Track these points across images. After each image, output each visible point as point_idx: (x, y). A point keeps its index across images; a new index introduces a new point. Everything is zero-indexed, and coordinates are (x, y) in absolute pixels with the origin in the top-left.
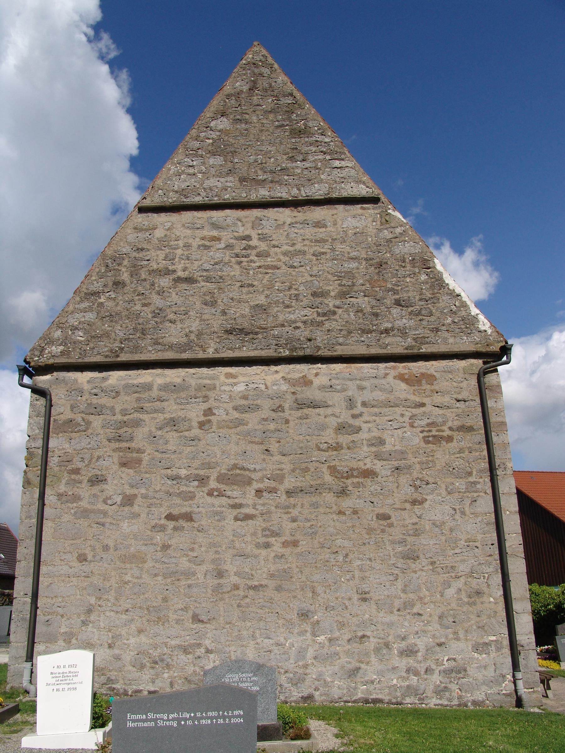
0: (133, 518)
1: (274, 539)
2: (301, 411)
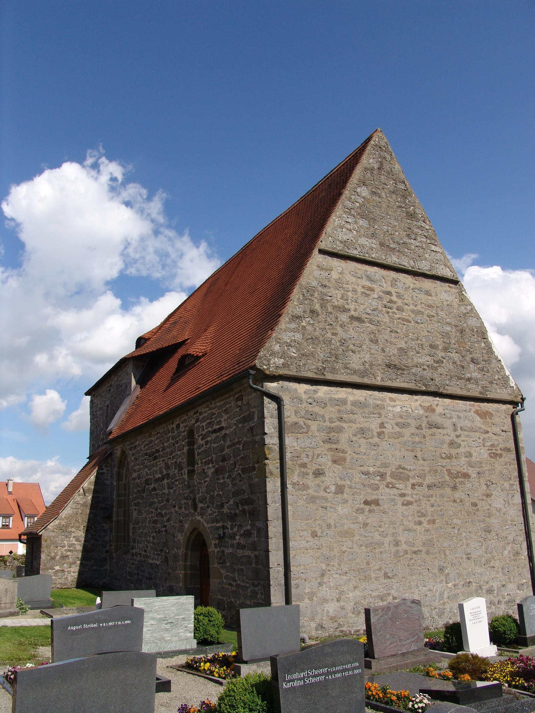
0: (344, 503)
1: (423, 518)
2: (431, 430)
